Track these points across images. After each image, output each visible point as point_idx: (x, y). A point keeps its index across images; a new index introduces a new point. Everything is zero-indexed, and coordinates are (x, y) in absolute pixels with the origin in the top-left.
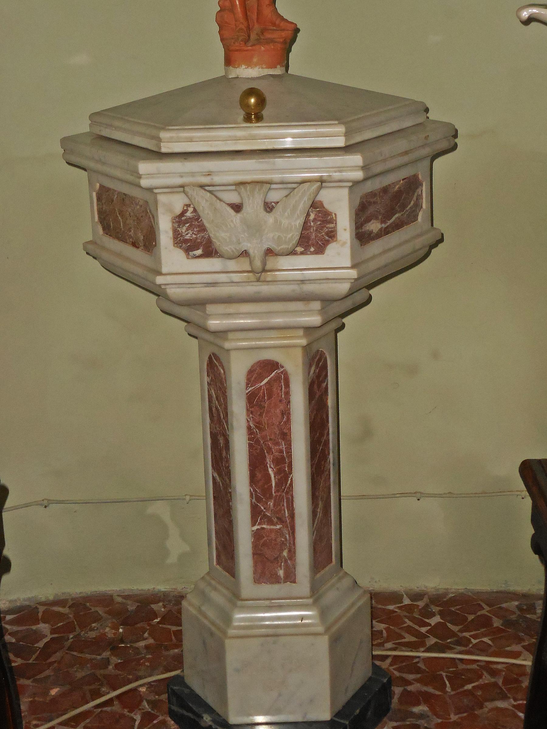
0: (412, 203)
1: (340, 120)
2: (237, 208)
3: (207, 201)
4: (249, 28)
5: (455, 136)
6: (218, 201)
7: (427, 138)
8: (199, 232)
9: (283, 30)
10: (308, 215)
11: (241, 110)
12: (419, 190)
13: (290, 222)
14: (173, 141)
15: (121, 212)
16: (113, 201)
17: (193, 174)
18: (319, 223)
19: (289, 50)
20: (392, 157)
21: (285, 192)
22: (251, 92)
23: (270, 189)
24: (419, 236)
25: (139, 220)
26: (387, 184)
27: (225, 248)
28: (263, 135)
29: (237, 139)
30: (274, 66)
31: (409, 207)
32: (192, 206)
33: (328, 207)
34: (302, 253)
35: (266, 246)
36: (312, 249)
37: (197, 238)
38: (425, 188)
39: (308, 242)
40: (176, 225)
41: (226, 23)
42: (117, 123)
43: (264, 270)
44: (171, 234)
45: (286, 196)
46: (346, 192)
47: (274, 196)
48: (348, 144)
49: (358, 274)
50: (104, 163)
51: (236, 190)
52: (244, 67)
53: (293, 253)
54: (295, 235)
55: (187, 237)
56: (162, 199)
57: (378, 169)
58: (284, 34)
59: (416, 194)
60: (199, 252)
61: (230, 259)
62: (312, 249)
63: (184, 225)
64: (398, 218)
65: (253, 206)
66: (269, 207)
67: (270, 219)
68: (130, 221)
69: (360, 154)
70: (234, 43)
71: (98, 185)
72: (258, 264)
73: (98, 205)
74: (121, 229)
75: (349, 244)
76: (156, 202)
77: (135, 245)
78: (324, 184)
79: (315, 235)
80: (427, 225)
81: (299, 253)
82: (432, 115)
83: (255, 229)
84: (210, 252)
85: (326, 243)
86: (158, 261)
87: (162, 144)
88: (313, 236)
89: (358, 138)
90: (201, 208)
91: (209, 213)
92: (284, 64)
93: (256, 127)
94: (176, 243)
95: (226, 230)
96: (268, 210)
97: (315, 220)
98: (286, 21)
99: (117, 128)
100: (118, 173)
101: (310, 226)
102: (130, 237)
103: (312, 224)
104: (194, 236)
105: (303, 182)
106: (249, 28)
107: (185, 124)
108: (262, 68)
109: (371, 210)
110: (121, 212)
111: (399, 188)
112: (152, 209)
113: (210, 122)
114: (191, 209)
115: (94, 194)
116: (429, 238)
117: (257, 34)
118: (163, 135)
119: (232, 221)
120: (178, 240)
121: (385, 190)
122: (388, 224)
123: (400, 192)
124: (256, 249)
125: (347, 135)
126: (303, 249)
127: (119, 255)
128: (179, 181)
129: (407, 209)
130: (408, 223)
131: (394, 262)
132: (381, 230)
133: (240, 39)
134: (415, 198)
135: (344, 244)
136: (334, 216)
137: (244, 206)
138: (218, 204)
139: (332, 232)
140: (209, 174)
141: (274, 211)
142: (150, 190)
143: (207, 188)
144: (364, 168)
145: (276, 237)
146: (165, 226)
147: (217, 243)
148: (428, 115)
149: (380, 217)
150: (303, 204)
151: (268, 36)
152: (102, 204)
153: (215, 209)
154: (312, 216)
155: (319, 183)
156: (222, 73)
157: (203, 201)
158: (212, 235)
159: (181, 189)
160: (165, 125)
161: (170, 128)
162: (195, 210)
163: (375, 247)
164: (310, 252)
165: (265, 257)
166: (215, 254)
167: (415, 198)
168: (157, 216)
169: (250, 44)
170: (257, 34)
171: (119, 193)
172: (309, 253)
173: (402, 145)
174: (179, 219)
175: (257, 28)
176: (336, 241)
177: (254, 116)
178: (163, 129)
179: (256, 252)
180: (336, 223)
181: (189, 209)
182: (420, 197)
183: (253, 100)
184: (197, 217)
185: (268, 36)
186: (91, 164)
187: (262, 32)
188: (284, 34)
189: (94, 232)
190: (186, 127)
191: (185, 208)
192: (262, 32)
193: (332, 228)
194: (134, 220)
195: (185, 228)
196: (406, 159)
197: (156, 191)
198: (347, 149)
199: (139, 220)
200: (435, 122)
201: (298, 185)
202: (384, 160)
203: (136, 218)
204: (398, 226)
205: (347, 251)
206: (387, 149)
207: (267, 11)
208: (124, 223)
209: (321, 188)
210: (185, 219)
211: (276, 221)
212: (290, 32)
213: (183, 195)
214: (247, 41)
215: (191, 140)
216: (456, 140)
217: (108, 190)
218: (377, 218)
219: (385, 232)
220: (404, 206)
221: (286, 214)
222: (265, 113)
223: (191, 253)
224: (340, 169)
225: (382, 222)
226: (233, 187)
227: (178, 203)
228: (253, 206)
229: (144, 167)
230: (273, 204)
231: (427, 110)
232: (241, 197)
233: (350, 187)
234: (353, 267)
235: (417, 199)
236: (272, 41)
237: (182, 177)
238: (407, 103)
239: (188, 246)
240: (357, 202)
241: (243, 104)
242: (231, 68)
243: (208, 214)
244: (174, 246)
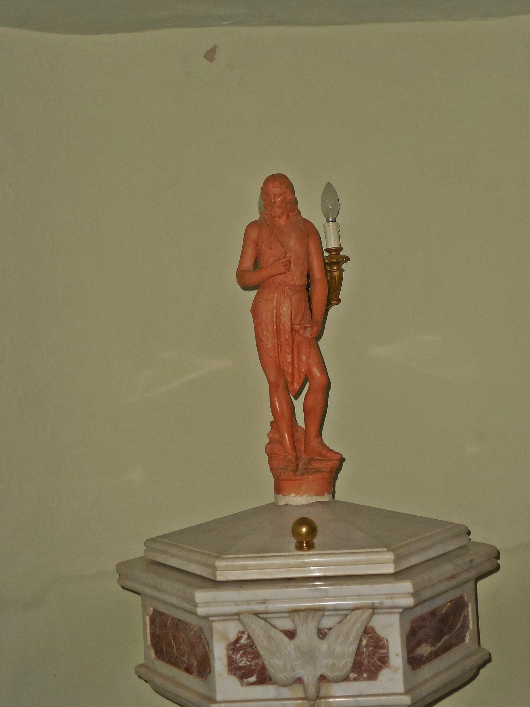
0: (460, 624)
1: (390, 549)
2: (291, 634)
3: (261, 628)
4: (297, 459)
5: (498, 557)
6: (272, 628)
7: (471, 561)
8: (253, 659)
9: (329, 460)
10: (361, 641)
11: (293, 538)
12: (465, 611)
13: (343, 649)
14: (227, 569)
15: (174, 637)
16: (166, 626)
17: (248, 602)
18: (371, 648)
19: (336, 478)
20: (440, 582)
21: (337, 619)
22: (303, 521)
23: (323, 615)
24: (466, 657)
25: (192, 646)
26: (439, 605)
27: (281, 676)
28: (315, 564)
29: (289, 566)
30: (321, 494)
31: (457, 627)
32: (246, 633)
33: (380, 632)
34: (355, 679)
35: (319, 674)
36: (365, 675)
37: (250, 665)
38: (470, 609)
39: (361, 668)
40: (230, 652)
41: (275, 454)
42: (172, 550)
43: (318, 697)
44: (225, 661)
45: (339, 623)
46: (397, 617)
47: (327, 622)
48: (397, 570)
49: (412, 701)
50: (160, 590)
51: (289, 617)
52: (293, 495)
53: (346, 679)
54: (347, 662)
55: (242, 664)
56: (217, 626)
57: (428, 593)
58: (330, 464)
59: (463, 615)
60: (253, 679)
61: (284, 686)
62: (365, 675)
63: (238, 652)
64: (447, 640)
65: (306, 633)
66: (322, 634)
67: (324, 646)
68: (184, 647)
69: (409, 581)
70: (284, 474)
71: (152, 609)
72: (312, 691)
73: (151, 628)
74: (174, 654)
75: (401, 670)
76: (211, 629)
77: (188, 670)
78: (376, 611)
79: (368, 661)
80: (475, 646)
81: (352, 679)
82: (474, 537)
83: (309, 656)
84: (264, 678)
85: (378, 669)
86: (213, 689)
87: (218, 573)
88: (366, 662)
89: (406, 564)
90: (256, 635)
91: (264, 640)
92: (331, 491)
93: (309, 555)
94: (231, 671)
95: (280, 657)
96: (321, 636)
97: (367, 646)
98: (332, 451)
99: (173, 555)
100: (174, 600)
101: (363, 652)
102: (183, 662)
103: (364, 649)
104: (248, 663)
105: (355, 609)
106: (297, 459)
107: (238, 553)
108: (311, 496)
109: (421, 634)
110: (174, 637)
111: (447, 610)
112: (207, 636)
113: (262, 550)
114: (245, 636)
115: (148, 618)
116: (476, 659)
117: (304, 464)
118: (219, 564)
119: (286, 648)
120: (233, 668)
121: (433, 613)
122: (437, 647)
123: (447, 614)
124: (309, 676)
125: (396, 561)
126: (356, 675)
127: (172, 680)
128: (234, 609)
129: (455, 630)
130: (456, 645)
131: (444, 686)
132: (431, 653)
133: (289, 469)
134: (462, 619)
135: (396, 670)
136: (385, 641)
137: (298, 635)
138: (273, 631)
139: (384, 657)
140: (264, 602)
141: (327, 637)
142: (206, 618)
143: (261, 616)
144: (415, 594)
145: (329, 665)
146: (219, 653)
147: (271, 671)
148: (470, 537)
149: (430, 640)
150: (357, 630)
151: (316, 465)
152: (156, 629)
153: (270, 636)
154: (364, 642)
155: (371, 611)
156: (273, 500)
157: (257, 629)
158: (266, 663)
159: (237, 617)
160: (220, 554)
161: (225, 556)
162: (249, 637)
163: (426, 671)
164: (364, 678)
165: (319, 684)
166: (269, 681)
167: (462, 619)
168: (212, 643)
169: (299, 473)
170: (304, 464)
171: (173, 618)
172: (362, 679)
173: (448, 569)
174: (234, 647)
175: (304, 458)
176: (389, 666)
177: (306, 544)
178: (218, 558)
179: (310, 678)
180: (388, 649)
181: (243, 636)
182: (466, 618)
183: (304, 530)
184: (251, 644)
185: (316, 465)
186: (147, 590)
187: (310, 461)
188: (330, 464)
189: (147, 657)
190: (241, 556)
191: (240, 635)
192: (310, 461)
193: (384, 654)
194: (188, 646)
195: (239, 655)
196: (453, 582)
197: (211, 619)
198: (397, 576)
199: (192, 646)
200: (477, 544)
201: (350, 611)
202: (433, 585)
203: (189, 644)
204: (447, 648)
205: (399, 676)
206: (434, 574)
207: (314, 443)
208: (178, 649)
209: (373, 614)
210: (240, 646)
211: (329, 647)
212: (336, 462)
213: (237, 622)
214: (295, 471)
215: (245, 568)
216: (499, 561)
217: (162, 614)
218: (427, 642)
219: (436, 655)
220: (451, 628)
221: (339, 640)
222: (316, 541)
223: (245, 680)
224: (391, 596)
225: (433, 645)
226: (287, 615)
227: (232, 630)
228: (306, 633)
229: (200, 596)
230: (326, 630)
231: (469, 533)
232: (295, 624)
233: (401, 613)
234: (407, 693)
235: (464, 620)
236: (319, 471)
237: (237, 605)
238: (450, 526)
239: (242, 673)
240: (408, 627)
241: (296, 533)
242: (281, 496)
243: (263, 641)
244: (242, 686)
